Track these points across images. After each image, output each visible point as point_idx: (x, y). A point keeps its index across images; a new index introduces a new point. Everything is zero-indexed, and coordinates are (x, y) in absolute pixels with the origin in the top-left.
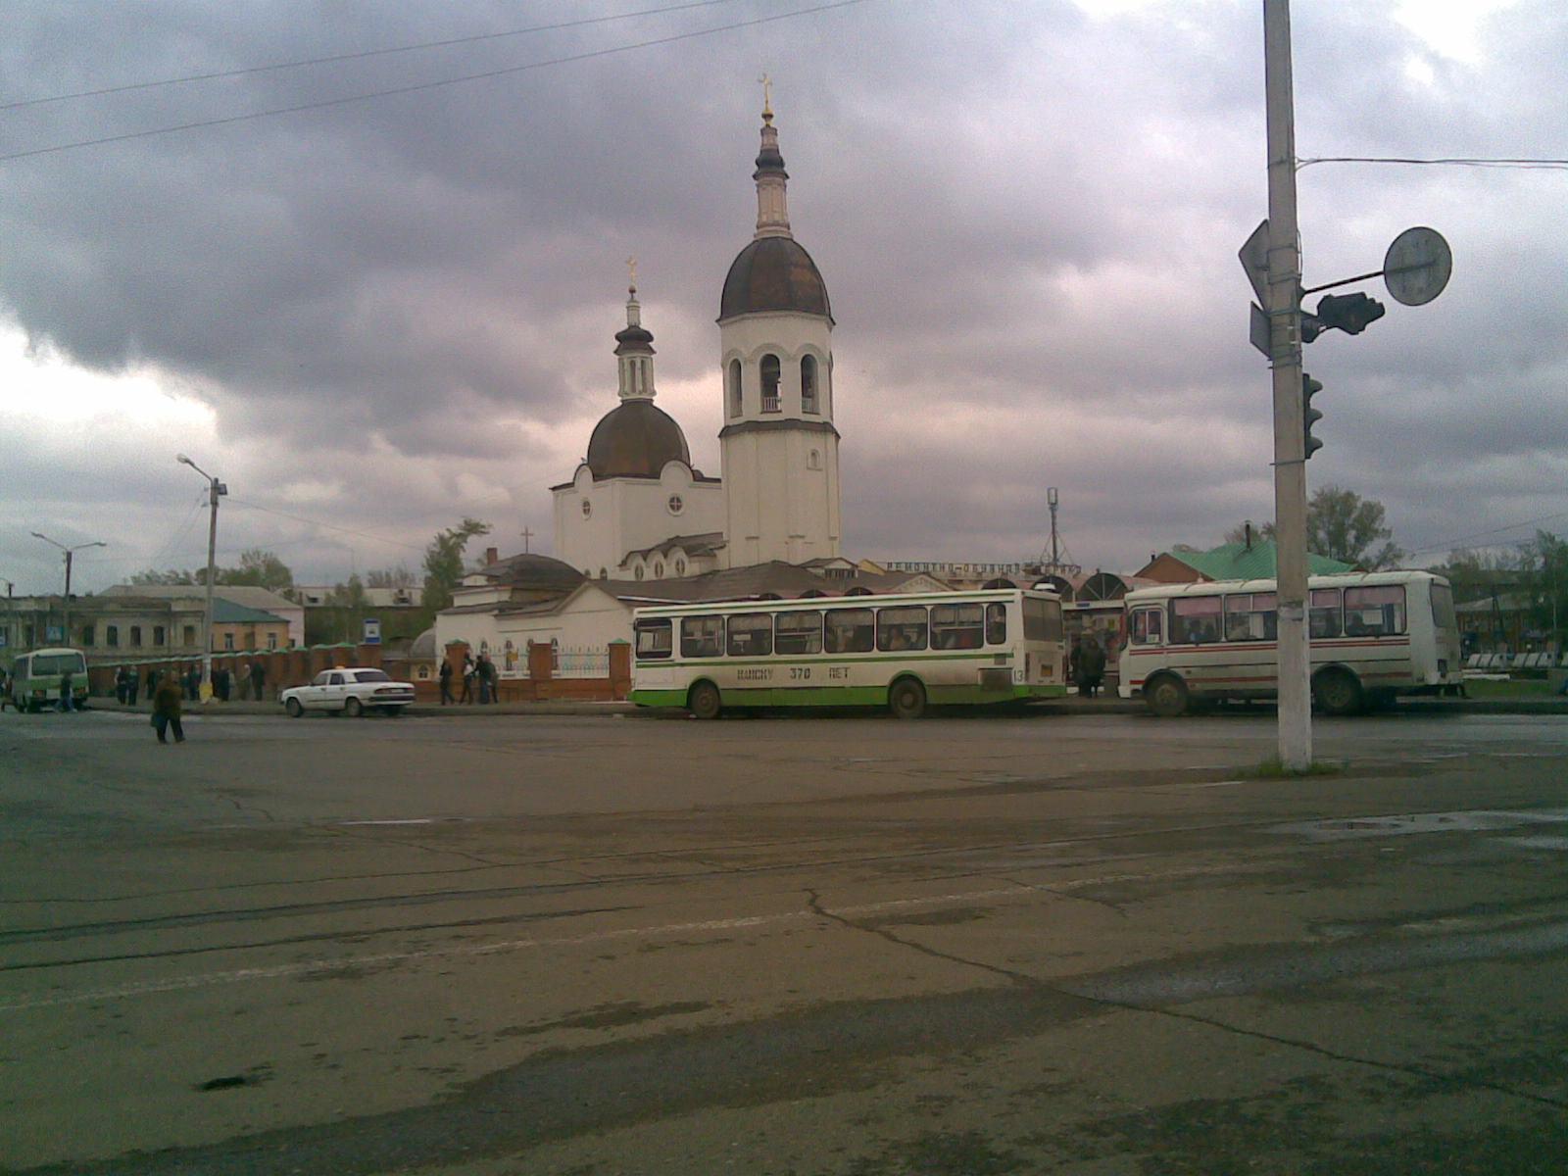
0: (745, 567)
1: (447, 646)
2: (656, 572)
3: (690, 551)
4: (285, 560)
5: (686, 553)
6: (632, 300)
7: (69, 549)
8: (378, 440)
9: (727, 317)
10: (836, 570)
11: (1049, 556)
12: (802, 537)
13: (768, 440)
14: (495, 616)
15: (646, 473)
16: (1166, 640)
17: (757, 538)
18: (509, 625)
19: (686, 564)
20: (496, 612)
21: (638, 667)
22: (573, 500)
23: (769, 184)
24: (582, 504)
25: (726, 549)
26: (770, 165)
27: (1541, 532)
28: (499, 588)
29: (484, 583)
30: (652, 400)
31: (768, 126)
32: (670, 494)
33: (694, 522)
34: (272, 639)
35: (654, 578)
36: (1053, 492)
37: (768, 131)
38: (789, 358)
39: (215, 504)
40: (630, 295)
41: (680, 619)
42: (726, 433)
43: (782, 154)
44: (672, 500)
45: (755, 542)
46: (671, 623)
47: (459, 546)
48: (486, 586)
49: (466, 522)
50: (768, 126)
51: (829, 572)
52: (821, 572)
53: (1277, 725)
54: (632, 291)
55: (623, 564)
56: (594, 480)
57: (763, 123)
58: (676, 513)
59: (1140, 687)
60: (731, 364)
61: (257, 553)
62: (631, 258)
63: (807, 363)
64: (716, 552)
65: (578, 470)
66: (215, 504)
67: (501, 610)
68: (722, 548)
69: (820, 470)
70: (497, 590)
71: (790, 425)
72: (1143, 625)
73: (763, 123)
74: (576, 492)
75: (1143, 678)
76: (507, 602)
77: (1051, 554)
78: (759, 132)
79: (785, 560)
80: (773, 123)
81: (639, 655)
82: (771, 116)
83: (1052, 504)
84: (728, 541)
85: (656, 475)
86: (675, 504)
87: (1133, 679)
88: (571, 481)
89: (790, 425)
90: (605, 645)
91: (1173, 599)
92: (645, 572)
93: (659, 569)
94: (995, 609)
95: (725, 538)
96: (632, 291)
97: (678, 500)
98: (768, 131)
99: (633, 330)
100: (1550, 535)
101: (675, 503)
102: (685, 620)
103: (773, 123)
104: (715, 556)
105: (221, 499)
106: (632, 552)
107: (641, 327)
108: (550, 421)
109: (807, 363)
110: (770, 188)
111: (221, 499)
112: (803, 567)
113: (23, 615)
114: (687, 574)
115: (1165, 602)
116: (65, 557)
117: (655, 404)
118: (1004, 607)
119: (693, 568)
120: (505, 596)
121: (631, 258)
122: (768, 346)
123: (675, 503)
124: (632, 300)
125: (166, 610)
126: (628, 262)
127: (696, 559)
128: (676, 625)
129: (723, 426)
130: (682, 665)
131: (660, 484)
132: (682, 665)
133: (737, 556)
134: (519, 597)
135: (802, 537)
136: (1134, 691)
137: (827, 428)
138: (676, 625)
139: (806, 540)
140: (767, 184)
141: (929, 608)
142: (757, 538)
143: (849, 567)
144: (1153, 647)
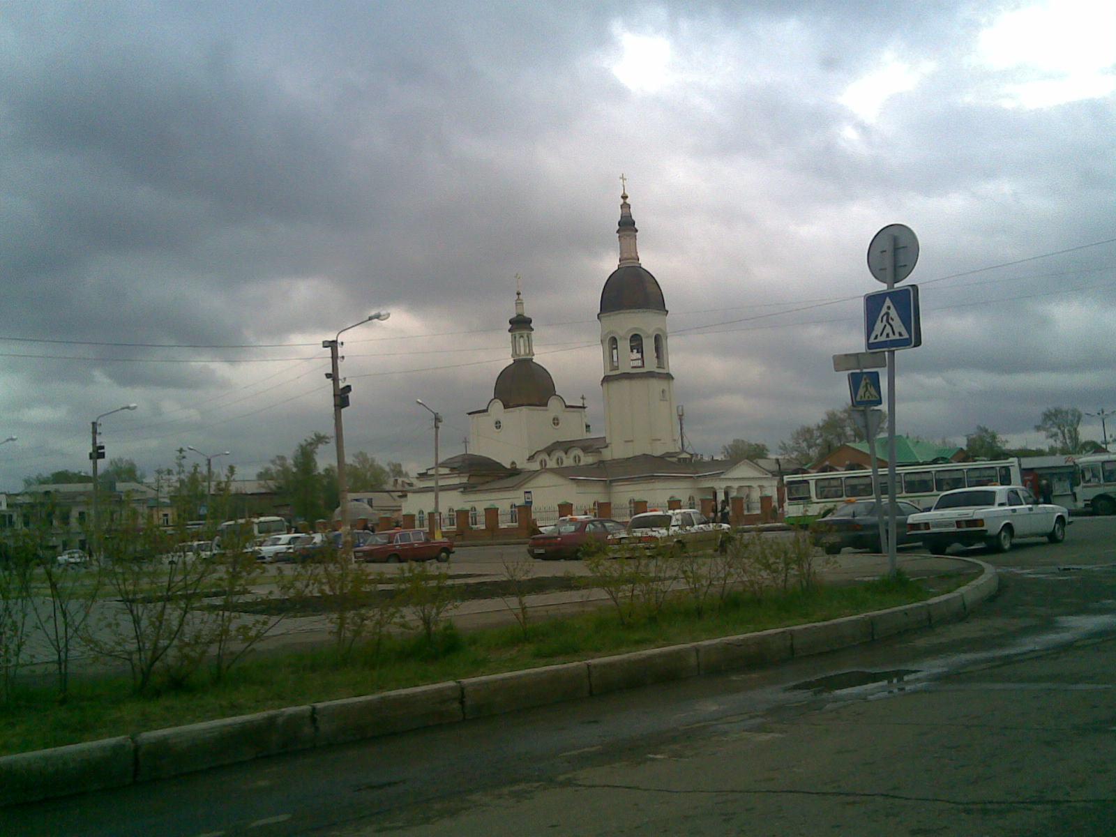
0: (624, 459)
1: (485, 509)
2: (558, 463)
3: (585, 449)
4: (135, 463)
5: (583, 451)
6: (519, 299)
7: (209, 458)
8: (98, 374)
9: (605, 313)
10: (683, 458)
11: (679, 448)
12: (659, 440)
13: (637, 384)
14: (462, 492)
15: (538, 403)
16: (1102, 481)
17: (632, 441)
18: (473, 497)
19: (564, 458)
20: (462, 489)
21: (789, 505)
22: (486, 421)
23: (629, 236)
24: (495, 422)
25: (609, 448)
26: (627, 225)
27: (980, 427)
28: (461, 475)
29: (450, 472)
30: (532, 359)
31: (625, 203)
32: (552, 415)
33: (572, 429)
34: (165, 518)
35: (558, 467)
36: (680, 408)
37: (625, 206)
38: (624, 338)
39: (437, 427)
40: (517, 296)
41: (814, 481)
42: (607, 379)
43: (633, 218)
44: (554, 419)
45: (631, 443)
46: (809, 483)
47: (313, 452)
48: (450, 474)
49: (316, 435)
50: (625, 203)
51: (679, 459)
52: (674, 460)
53: (898, 534)
54: (518, 294)
55: (531, 458)
56: (505, 408)
57: (622, 201)
58: (556, 427)
59: (1089, 502)
60: (610, 339)
61: (121, 460)
62: (517, 274)
63: (658, 339)
64: (602, 450)
65: (490, 402)
66: (437, 427)
67: (465, 488)
68: (606, 447)
69: (667, 400)
70: (459, 476)
71: (651, 375)
72: (1088, 475)
73: (622, 201)
74: (489, 415)
75: (1091, 498)
76: (466, 483)
77: (681, 446)
78: (620, 207)
79: (650, 453)
80: (628, 201)
81: (789, 499)
82: (627, 197)
83: (680, 416)
84: (610, 443)
85: (546, 405)
86: (556, 422)
87: (1085, 498)
88: (485, 408)
89: (651, 375)
90: (483, 509)
91: (1104, 463)
92: (548, 463)
93: (560, 461)
94: (1003, 470)
95: (608, 441)
96: (518, 294)
97: (557, 420)
98: (625, 206)
99: (520, 317)
100: (984, 428)
101: (556, 421)
102: (817, 481)
103: (628, 201)
104: (601, 452)
105: (440, 425)
106: (538, 451)
107: (525, 315)
108: (231, 361)
109: (658, 339)
110: (628, 238)
111: (440, 425)
112: (662, 457)
113: (21, 505)
114: (582, 463)
115: (1100, 464)
116: (207, 462)
117: (534, 361)
118: (1009, 470)
119: (587, 459)
120: (465, 480)
121: (517, 274)
122: (635, 329)
123: (556, 421)
124: (519, 299)
125: (118, 499)
126: (516, 277)
127: (590, 454)
128: (812, 484)
129: (603, 376)
130: (818, 503)
131: (546, 410)
132: (818, 503)
133: (616, 451)
134: (473, 480)
135: (659, 440)
136: (1086, 505)
137: (669, 377)
138: (812, 484)
139: (662, 441)
140: (627, 236)
141: (933, 472)
142: (632, 441)
143: (689, 456)
144: (1094, 484)
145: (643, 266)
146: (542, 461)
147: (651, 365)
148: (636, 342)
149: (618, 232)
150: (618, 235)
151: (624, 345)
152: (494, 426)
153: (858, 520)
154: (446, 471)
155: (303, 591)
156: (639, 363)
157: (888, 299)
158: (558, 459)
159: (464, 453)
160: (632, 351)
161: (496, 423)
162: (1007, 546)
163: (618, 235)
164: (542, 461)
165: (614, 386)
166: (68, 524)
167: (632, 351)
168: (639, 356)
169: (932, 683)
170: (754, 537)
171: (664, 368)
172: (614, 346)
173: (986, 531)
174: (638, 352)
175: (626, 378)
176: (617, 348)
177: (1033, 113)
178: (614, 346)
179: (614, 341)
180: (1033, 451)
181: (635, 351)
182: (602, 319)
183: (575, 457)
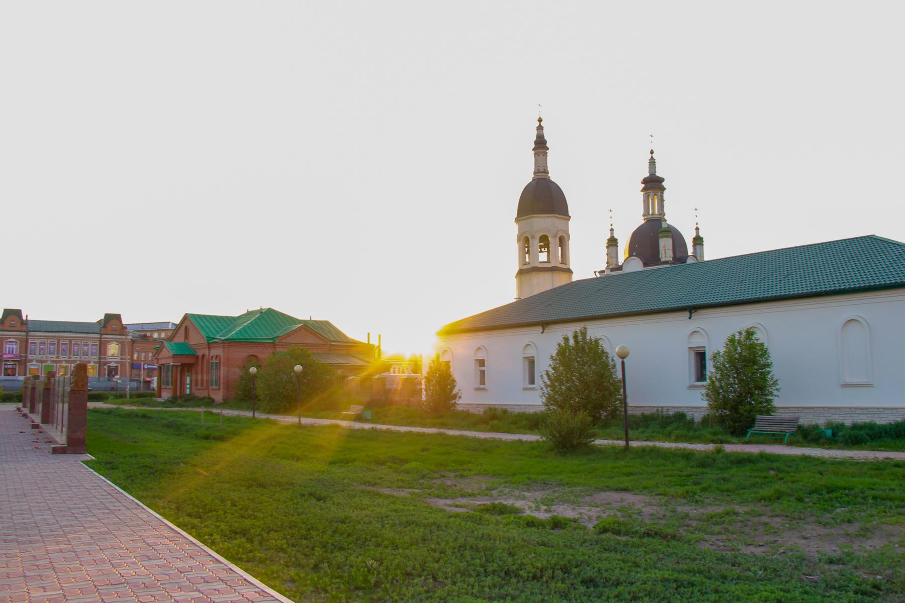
31: (540, 125)
50: (540, 125)
71: (554, 269)
73: (538, 124)
80: (542, 124)
98: (540, 128)
103: (542, 124)
145: (552, 179)
147: (556, 262)
148: (545, 241)
149: (534, 149)
150: (534, 152)
153: (427, 395)
163: (534, 152)
166: (491, 420)
170: (739, 550)
171: (566, 264)
173: (371, 375)
175: (535, 271)
177: (604, 358)
179: (527, 240)
180: (877, 425)
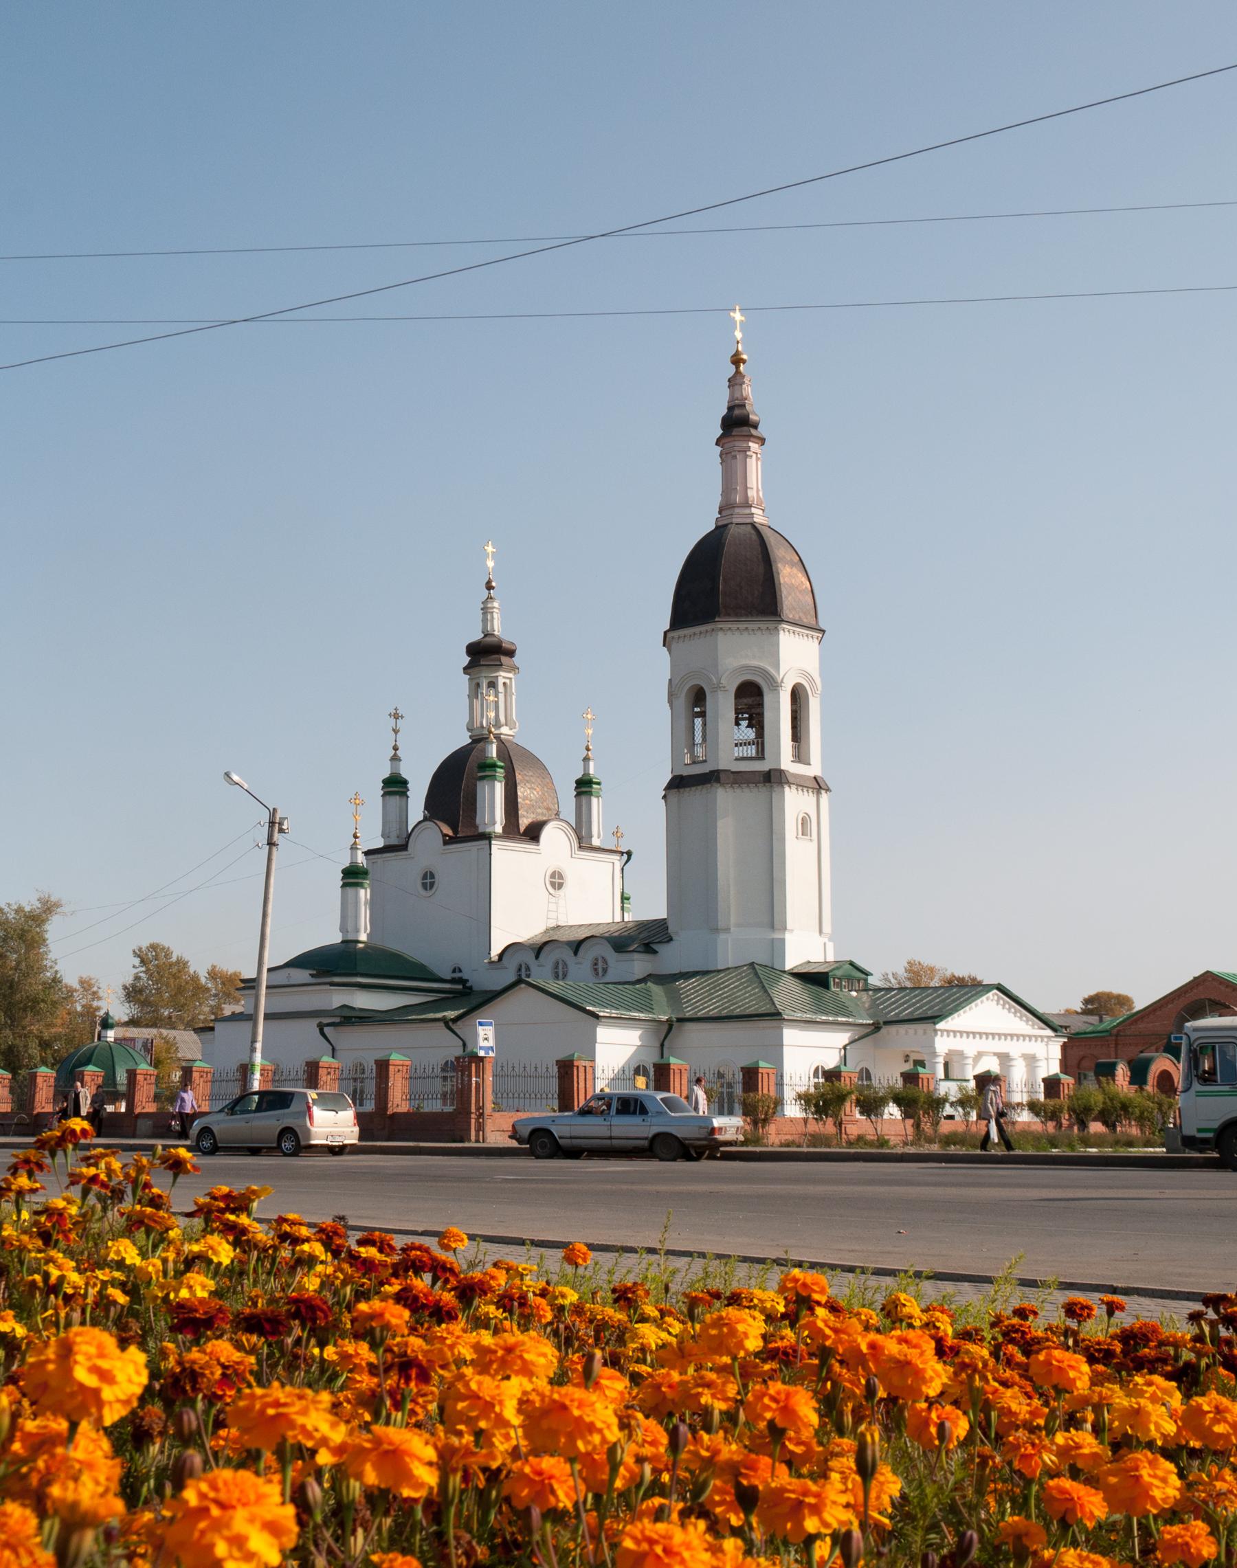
59: (1210, 1135)
99: (488, 639)
101: (557, 881)
123: (557, 881)
129: (670, 777)
146: (558, 963)
151: (723, 705)
152: (419, 882)
154: (302, 975)
155: (335, 1345)
156: (751, 751)
157: (522, 829)
158: (557, 967)
159: (335, 938)
160: (737, 724)
161: (425, 877)
162: (497, 1132)
163: (719, 449)
164: (521, 966)
165: (694, 797)
167: (737, 724)
168: (751, 734)
169: (903, 1429)
172: (697, 709)
174: (749, 726)
176: (702, 714)
178: (697, 709)
179: (699, 697)
181: (744, 723)
182: (674, 646)
183: (556, 966)
